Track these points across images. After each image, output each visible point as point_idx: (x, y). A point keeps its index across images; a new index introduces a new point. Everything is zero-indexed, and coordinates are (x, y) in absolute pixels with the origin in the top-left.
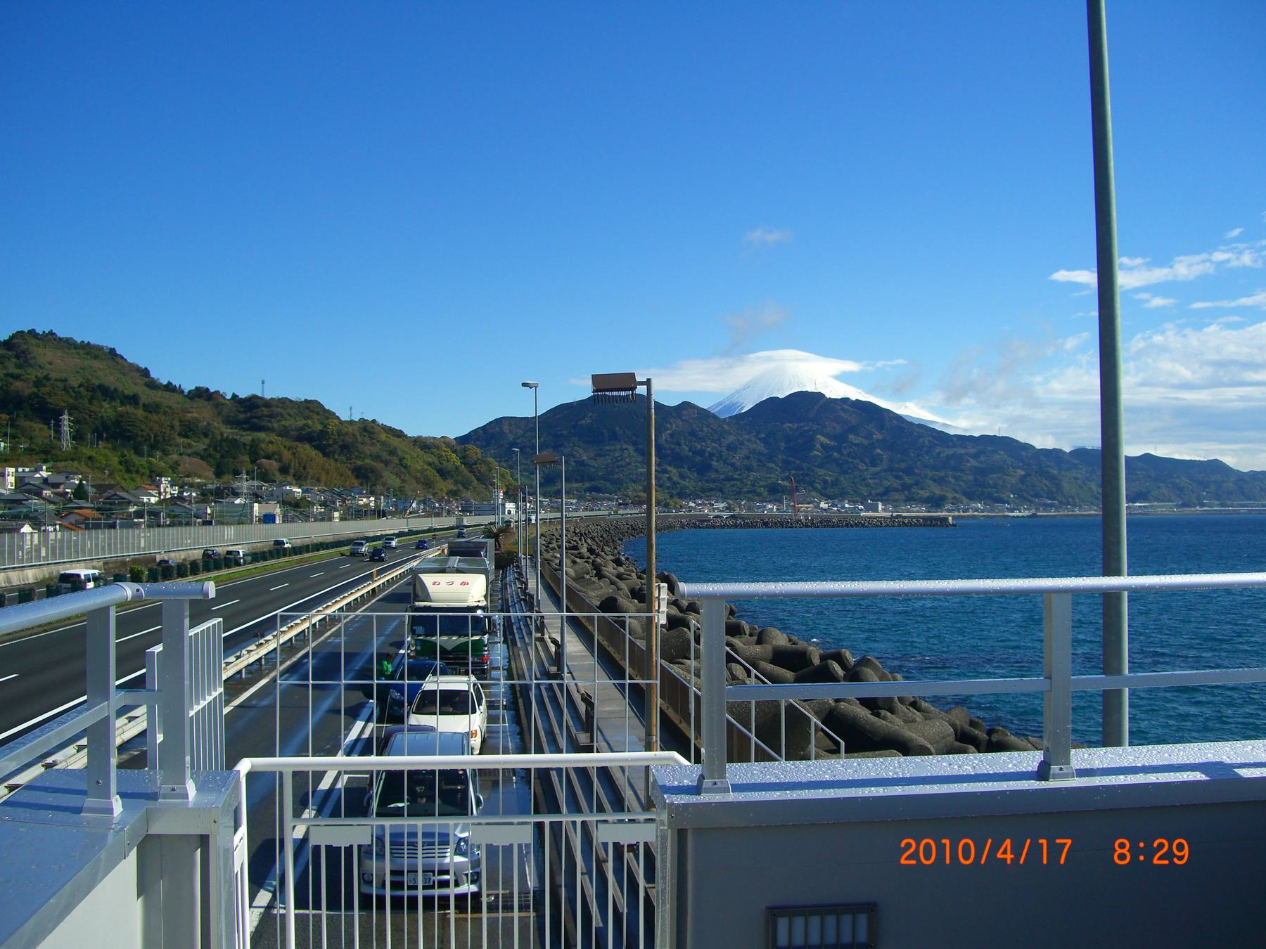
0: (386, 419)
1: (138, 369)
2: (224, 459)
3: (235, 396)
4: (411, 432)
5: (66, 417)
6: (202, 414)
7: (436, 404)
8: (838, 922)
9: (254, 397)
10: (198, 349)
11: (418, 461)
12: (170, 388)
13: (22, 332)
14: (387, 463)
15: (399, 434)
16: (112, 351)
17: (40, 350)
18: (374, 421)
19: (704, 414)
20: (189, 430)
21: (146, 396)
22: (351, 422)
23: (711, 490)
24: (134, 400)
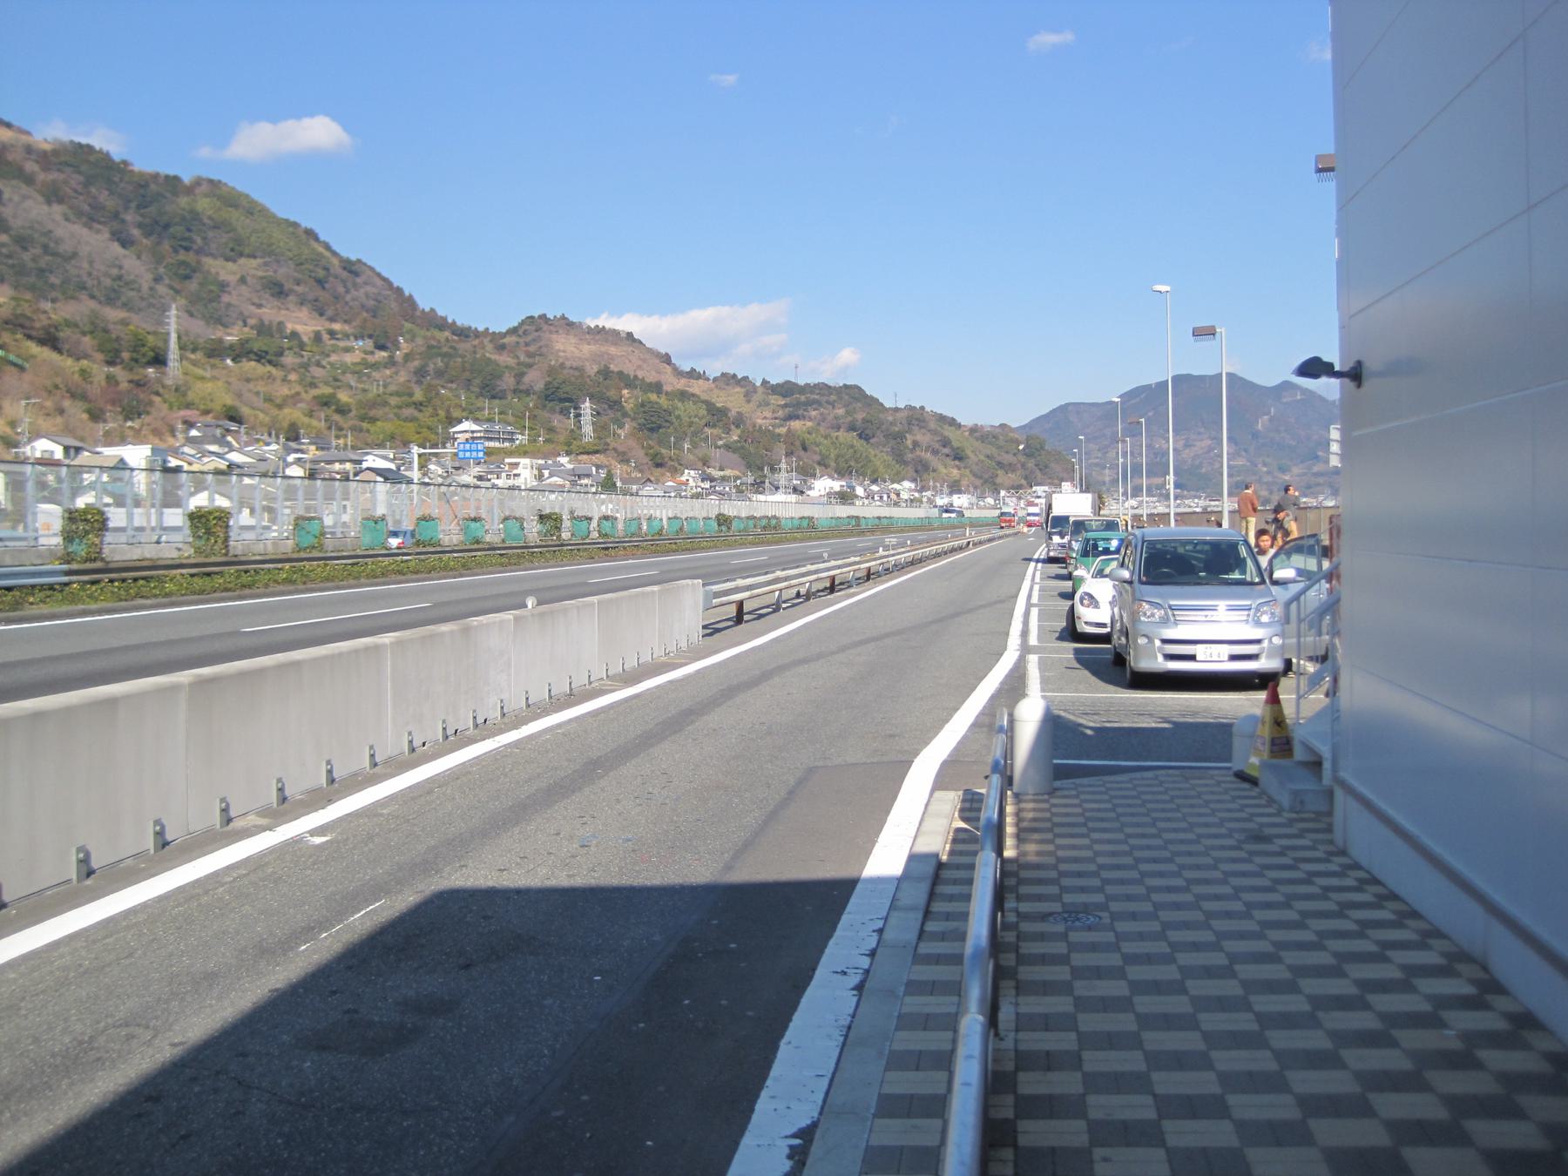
0: (935, 404)
1: (657, 355)
2: (654, 423)
3: (765, 382)
4: (966, 420)
5: (587, 404)
6: (732, 401)
7: (990, 391)
8: (1298, 712)
9: (788, 382)
10: (705, 326)
11: (976, 453)
12: (693, 374)
13: (532, 317)
14: (935, 452)
15: (952, 422)
16: (630, 335)
17: (554, 336)
18: (922, 408)
19: (306, 116)
20: (717, 415)
21: (672, 383)
22: (897, 410)
23: (1318, 484)
24: (657, 387)
